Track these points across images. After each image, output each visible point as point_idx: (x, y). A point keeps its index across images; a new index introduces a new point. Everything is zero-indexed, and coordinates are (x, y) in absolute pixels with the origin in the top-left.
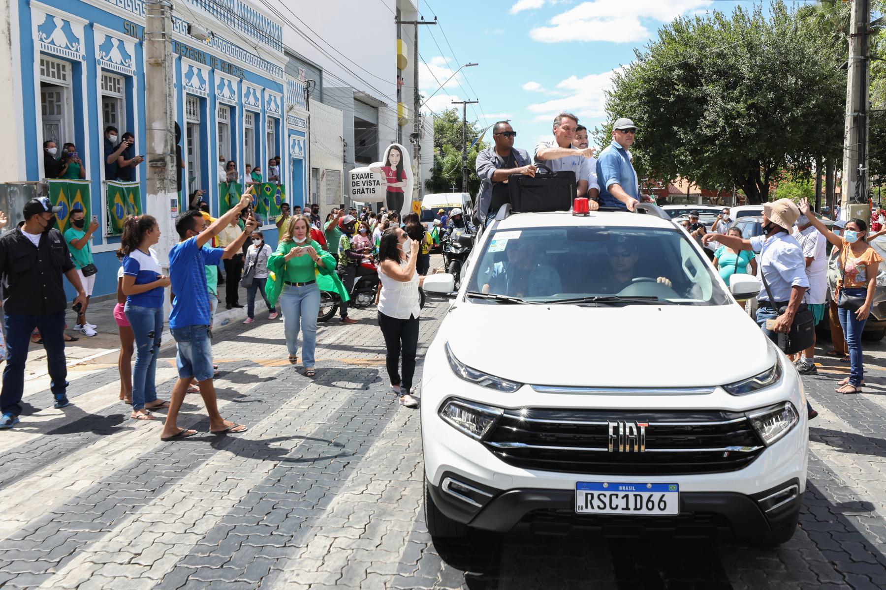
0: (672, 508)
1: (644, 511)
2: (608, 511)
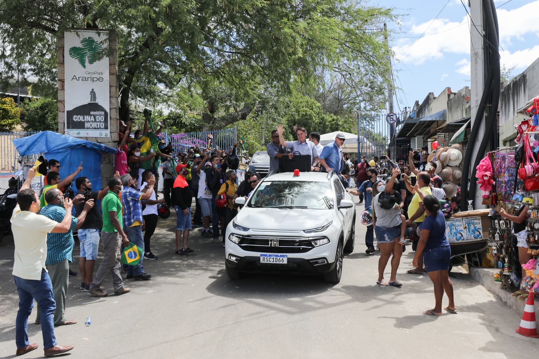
0: (285, 262)
1: (278, 262)
2: (269, 262)
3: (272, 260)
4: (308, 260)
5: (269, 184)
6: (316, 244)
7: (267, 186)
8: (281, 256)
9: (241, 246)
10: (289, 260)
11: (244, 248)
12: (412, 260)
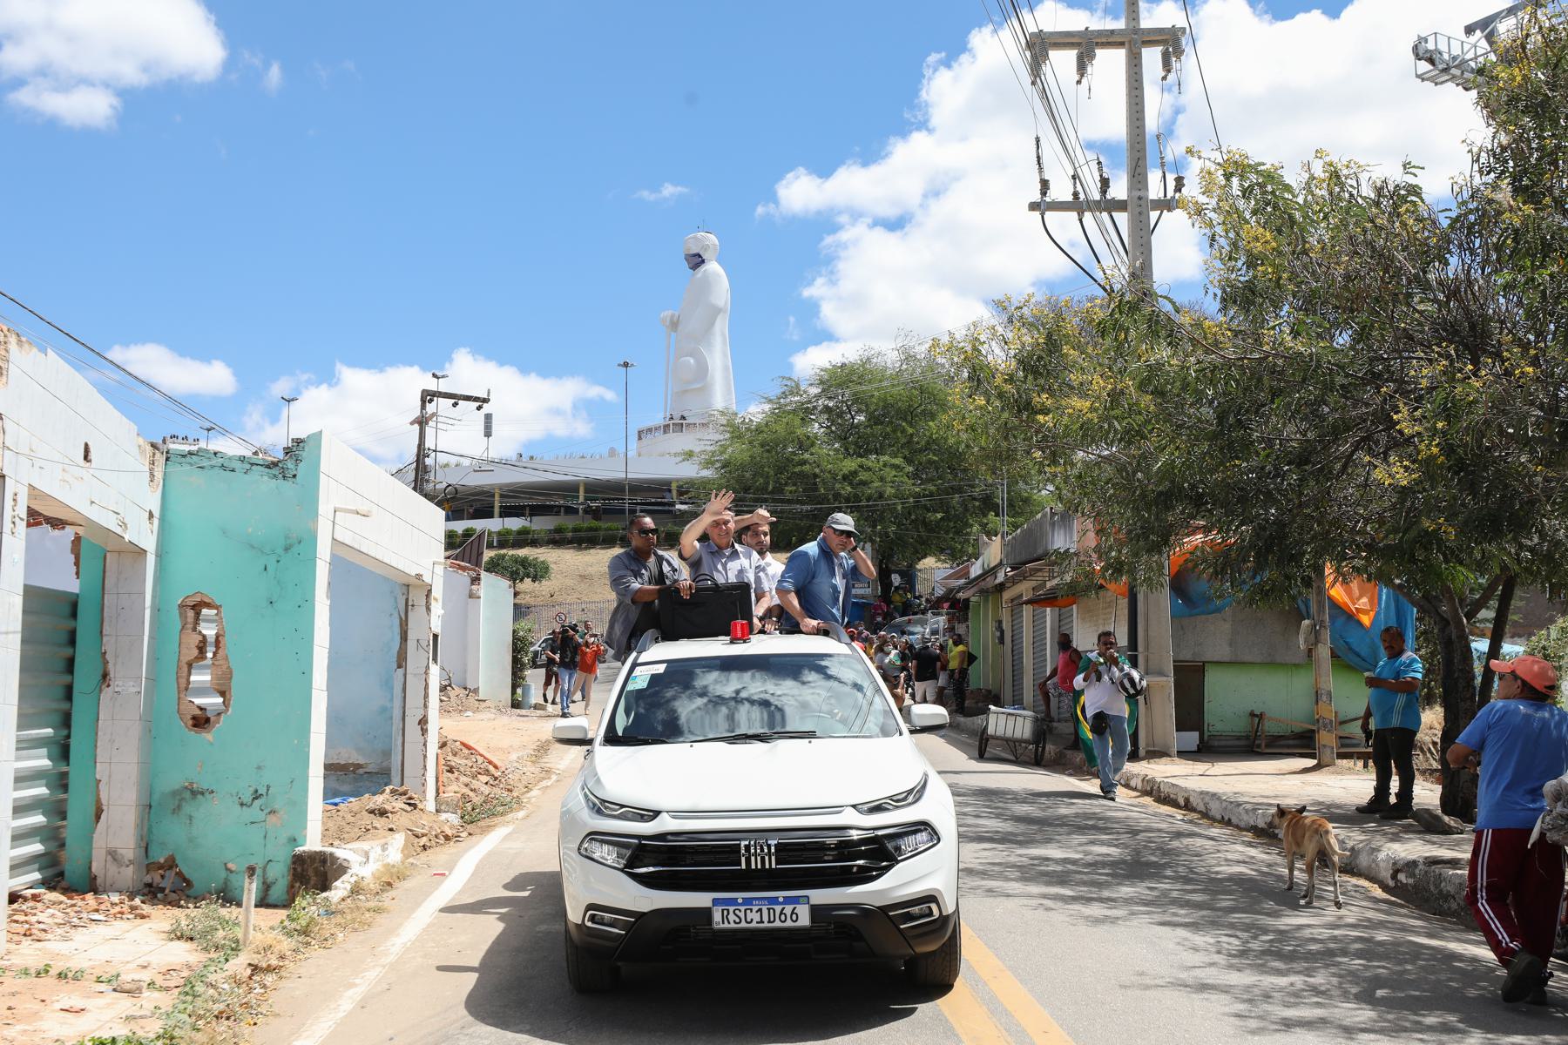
0: (804, 920)
1: (778, 924)
3: (757, 917)
4: (884, 910)
5: (661, 668)
6: (898, 849)
7: (654, 679)
8: (788, 900)
9: (635, 877)
10: (816, 911)
11: (648, 881)
12: (817, 289)
